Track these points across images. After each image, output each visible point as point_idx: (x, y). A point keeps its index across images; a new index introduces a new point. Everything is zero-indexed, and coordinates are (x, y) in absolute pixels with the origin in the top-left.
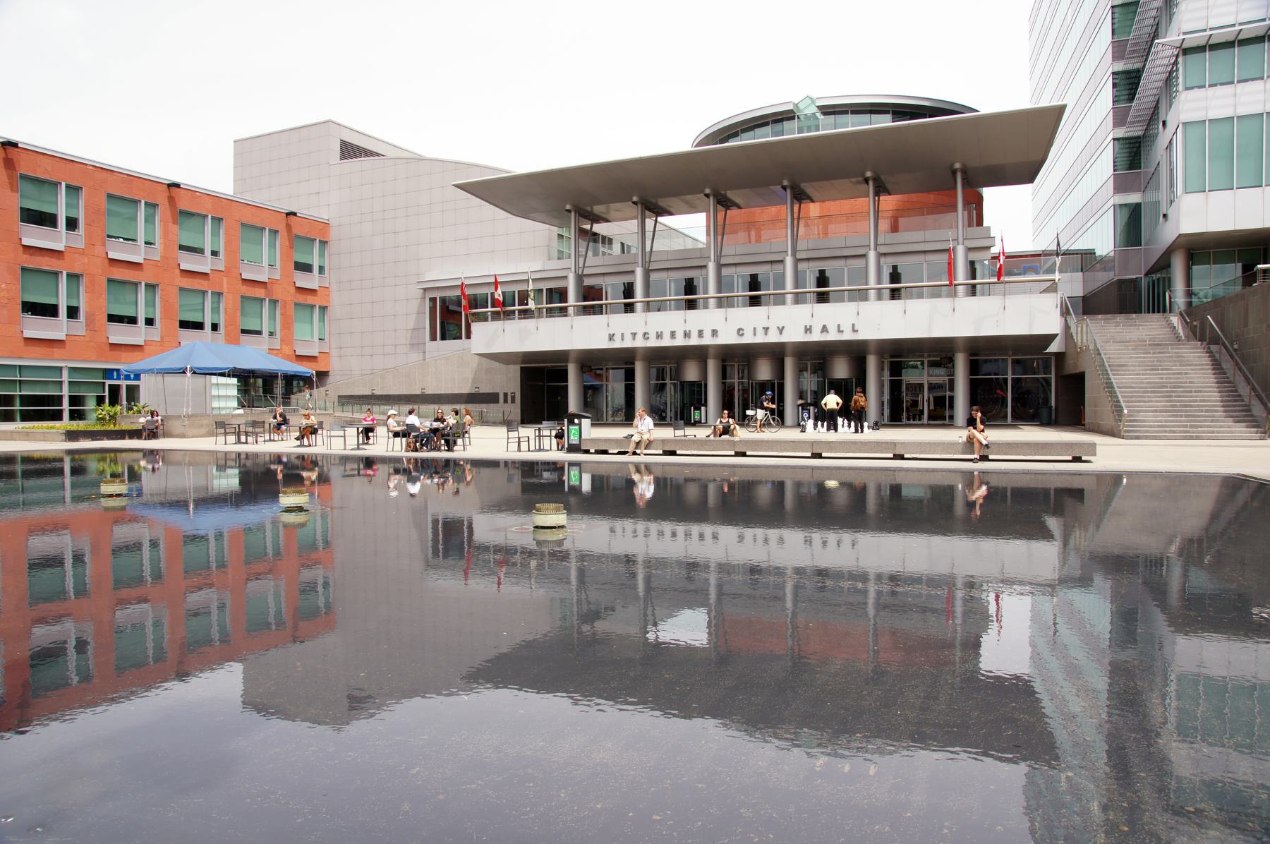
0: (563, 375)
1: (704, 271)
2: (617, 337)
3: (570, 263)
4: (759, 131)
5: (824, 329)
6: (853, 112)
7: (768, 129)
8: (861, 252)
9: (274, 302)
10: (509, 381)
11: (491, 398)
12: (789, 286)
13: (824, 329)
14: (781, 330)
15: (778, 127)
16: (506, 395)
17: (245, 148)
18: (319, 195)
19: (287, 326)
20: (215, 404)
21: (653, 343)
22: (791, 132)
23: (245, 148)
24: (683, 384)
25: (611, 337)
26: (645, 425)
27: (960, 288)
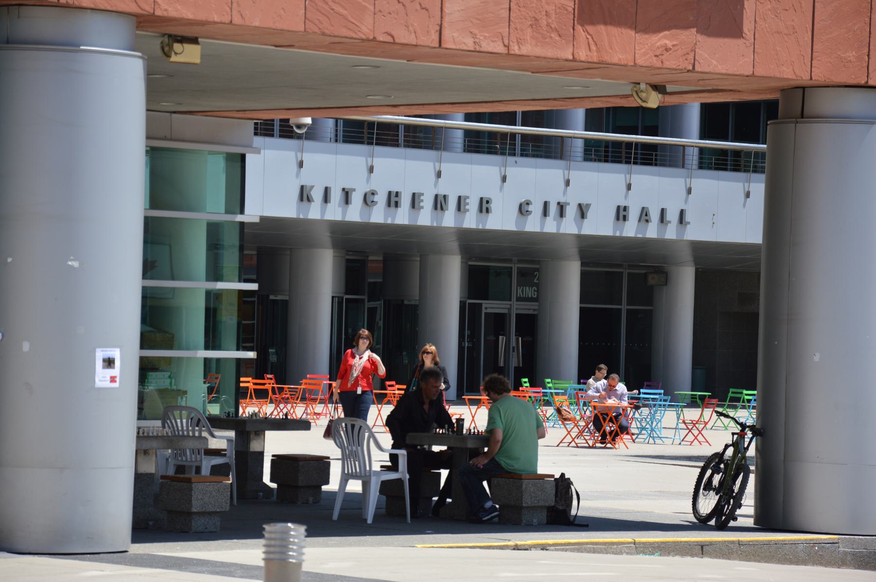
13: (644, 216)
14: (582, 211)
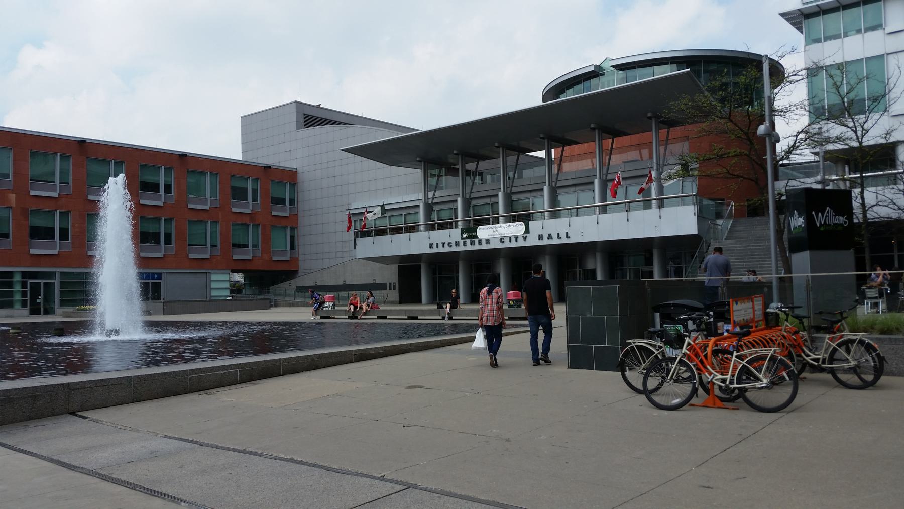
0: (418, 270)
1: (455, 204)
2: (434, 246)
3: (421, 196)
4: (576, 88)
5: (550, 237)
6: (639, 67)
7: (580, 87)
8: (589, 180)
9: (256, 226)
10: (390, 274)
11: (382, 287)
12: (654, 195)
13: (550, 237)
15: (587, 84)
16: (390, 284)
17: (248, 121)
18: (290, 151)
19: (267, 240)
20: (214, 293)
21: (555, 241)
22: (601, 86)
23: (248, 121)
24: (584, 270)
25: (431, 246)
26: (425, 306)
27: (654, 202)
